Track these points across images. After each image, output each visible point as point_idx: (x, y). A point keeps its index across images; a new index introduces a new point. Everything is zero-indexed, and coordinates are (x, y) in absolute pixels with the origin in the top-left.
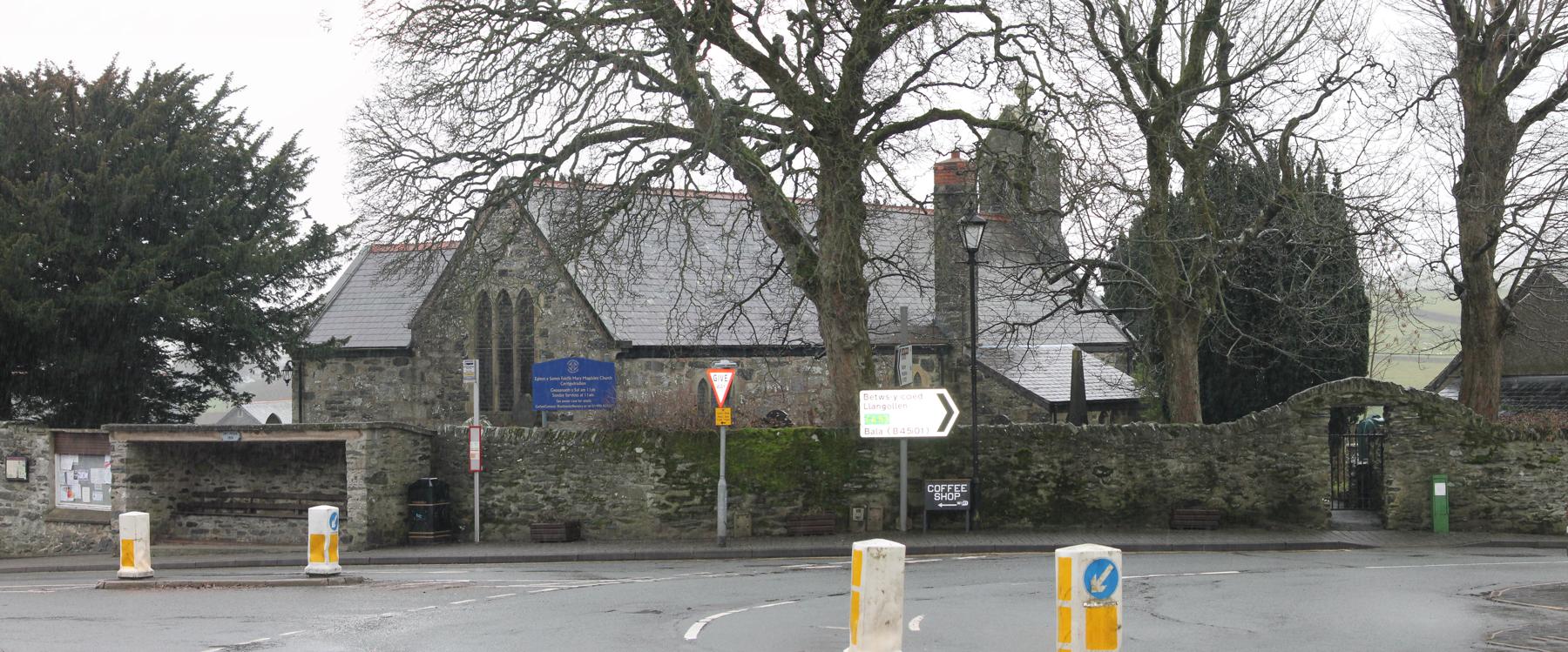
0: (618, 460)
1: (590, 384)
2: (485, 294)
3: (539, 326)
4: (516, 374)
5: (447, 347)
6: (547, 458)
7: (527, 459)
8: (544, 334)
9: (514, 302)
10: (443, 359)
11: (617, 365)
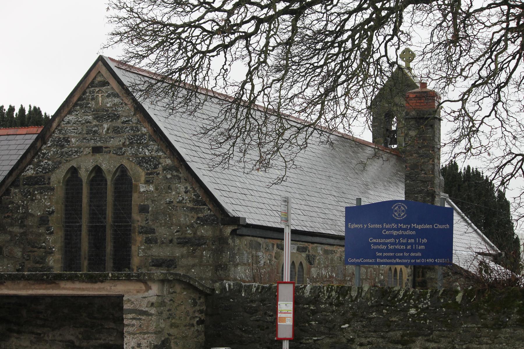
0: (499, 325)
1: (421, 233)
2: (74, 171)
3: (136, 200)
4: (109, 248)
5: (29, 222)
6: (388, 325)
7: (357, 325)
8: (144, 209)
9: (109, 178)
10: (24, 234)
11: (230, 241)
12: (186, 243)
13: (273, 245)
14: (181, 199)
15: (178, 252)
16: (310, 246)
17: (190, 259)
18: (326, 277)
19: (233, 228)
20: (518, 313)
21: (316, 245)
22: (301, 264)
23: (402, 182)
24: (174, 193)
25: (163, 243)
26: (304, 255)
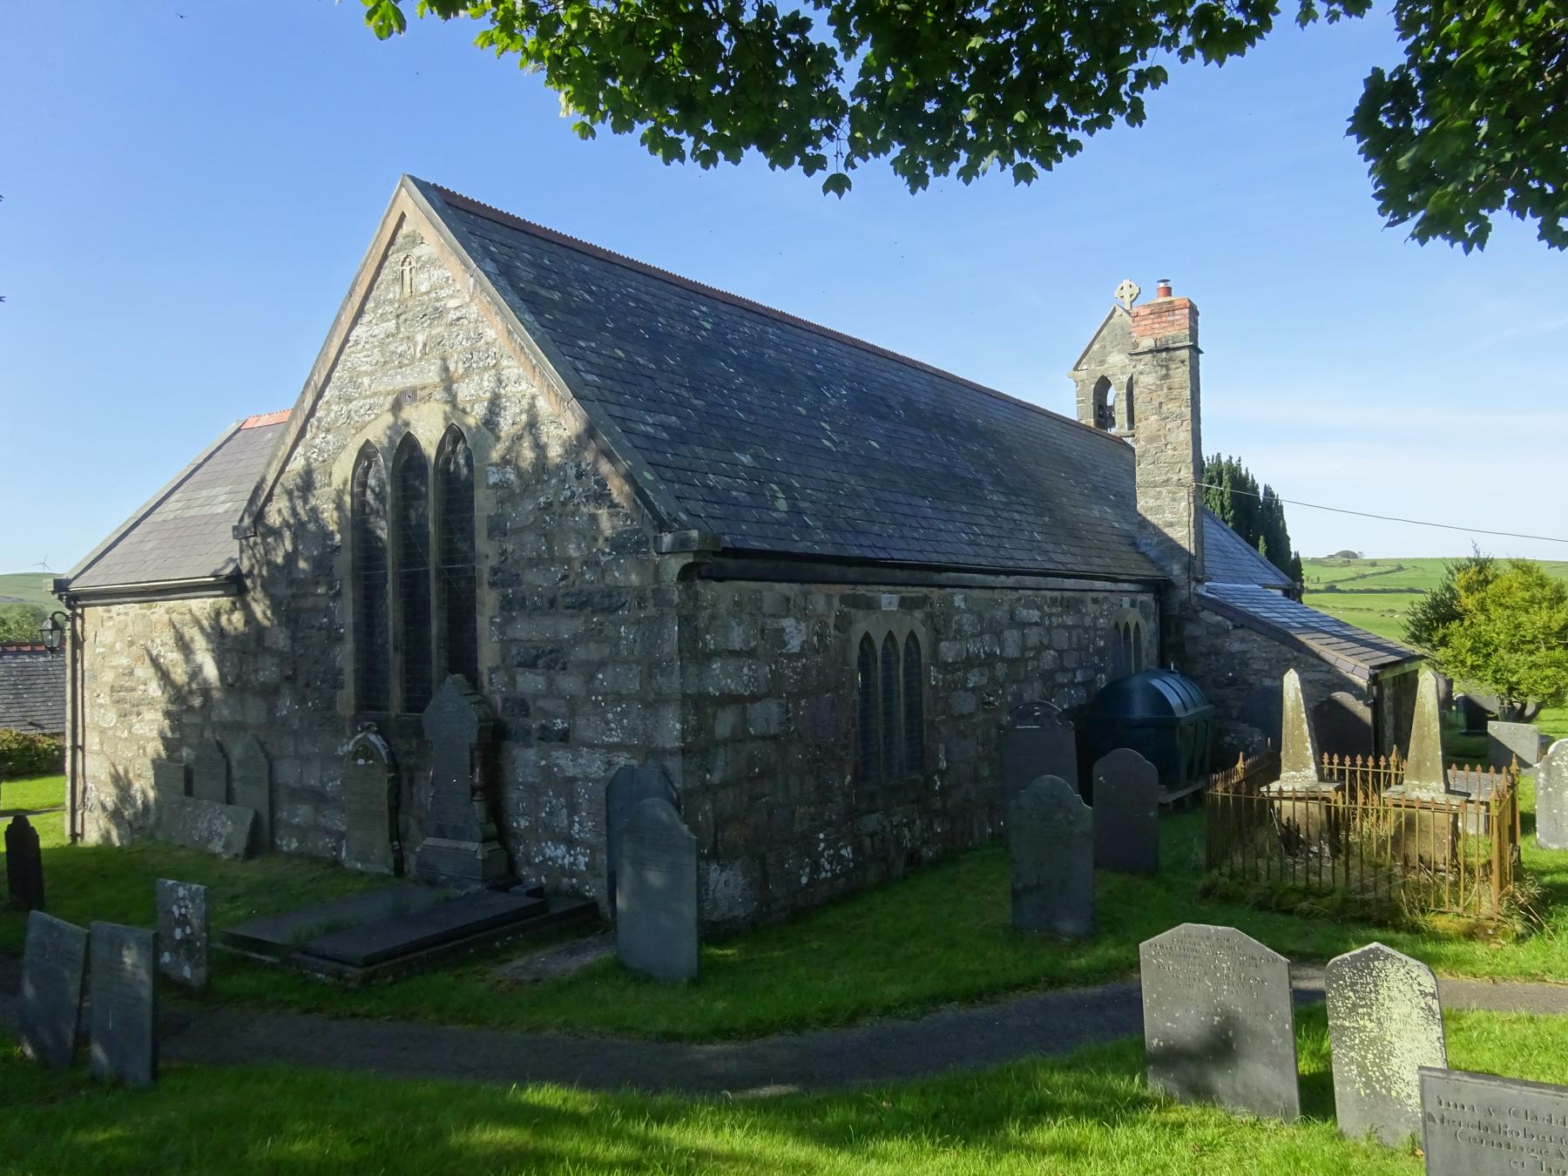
12: (582, 606)
13: (829, 597)
14: (568, 493)
15: (567, 627)
16: (935, 593)
17: (593, 646)
18: (978, 656)
19: (685, 562)
20: (1560, 66)
21: (949, 590)
22: (912, 635)
23: (1314, 562)
24: (554, 481)
25: (536, 608)
26: (919, 614)
